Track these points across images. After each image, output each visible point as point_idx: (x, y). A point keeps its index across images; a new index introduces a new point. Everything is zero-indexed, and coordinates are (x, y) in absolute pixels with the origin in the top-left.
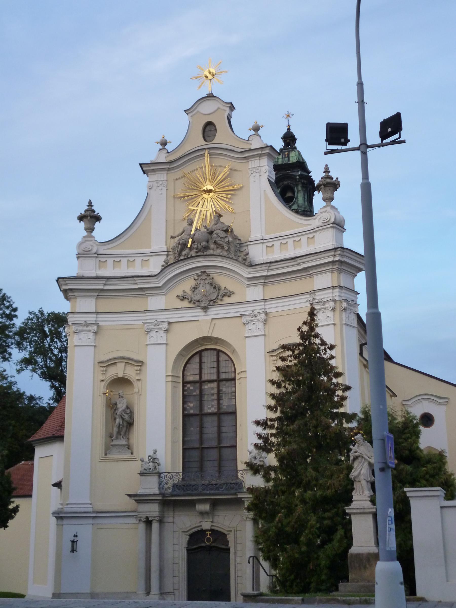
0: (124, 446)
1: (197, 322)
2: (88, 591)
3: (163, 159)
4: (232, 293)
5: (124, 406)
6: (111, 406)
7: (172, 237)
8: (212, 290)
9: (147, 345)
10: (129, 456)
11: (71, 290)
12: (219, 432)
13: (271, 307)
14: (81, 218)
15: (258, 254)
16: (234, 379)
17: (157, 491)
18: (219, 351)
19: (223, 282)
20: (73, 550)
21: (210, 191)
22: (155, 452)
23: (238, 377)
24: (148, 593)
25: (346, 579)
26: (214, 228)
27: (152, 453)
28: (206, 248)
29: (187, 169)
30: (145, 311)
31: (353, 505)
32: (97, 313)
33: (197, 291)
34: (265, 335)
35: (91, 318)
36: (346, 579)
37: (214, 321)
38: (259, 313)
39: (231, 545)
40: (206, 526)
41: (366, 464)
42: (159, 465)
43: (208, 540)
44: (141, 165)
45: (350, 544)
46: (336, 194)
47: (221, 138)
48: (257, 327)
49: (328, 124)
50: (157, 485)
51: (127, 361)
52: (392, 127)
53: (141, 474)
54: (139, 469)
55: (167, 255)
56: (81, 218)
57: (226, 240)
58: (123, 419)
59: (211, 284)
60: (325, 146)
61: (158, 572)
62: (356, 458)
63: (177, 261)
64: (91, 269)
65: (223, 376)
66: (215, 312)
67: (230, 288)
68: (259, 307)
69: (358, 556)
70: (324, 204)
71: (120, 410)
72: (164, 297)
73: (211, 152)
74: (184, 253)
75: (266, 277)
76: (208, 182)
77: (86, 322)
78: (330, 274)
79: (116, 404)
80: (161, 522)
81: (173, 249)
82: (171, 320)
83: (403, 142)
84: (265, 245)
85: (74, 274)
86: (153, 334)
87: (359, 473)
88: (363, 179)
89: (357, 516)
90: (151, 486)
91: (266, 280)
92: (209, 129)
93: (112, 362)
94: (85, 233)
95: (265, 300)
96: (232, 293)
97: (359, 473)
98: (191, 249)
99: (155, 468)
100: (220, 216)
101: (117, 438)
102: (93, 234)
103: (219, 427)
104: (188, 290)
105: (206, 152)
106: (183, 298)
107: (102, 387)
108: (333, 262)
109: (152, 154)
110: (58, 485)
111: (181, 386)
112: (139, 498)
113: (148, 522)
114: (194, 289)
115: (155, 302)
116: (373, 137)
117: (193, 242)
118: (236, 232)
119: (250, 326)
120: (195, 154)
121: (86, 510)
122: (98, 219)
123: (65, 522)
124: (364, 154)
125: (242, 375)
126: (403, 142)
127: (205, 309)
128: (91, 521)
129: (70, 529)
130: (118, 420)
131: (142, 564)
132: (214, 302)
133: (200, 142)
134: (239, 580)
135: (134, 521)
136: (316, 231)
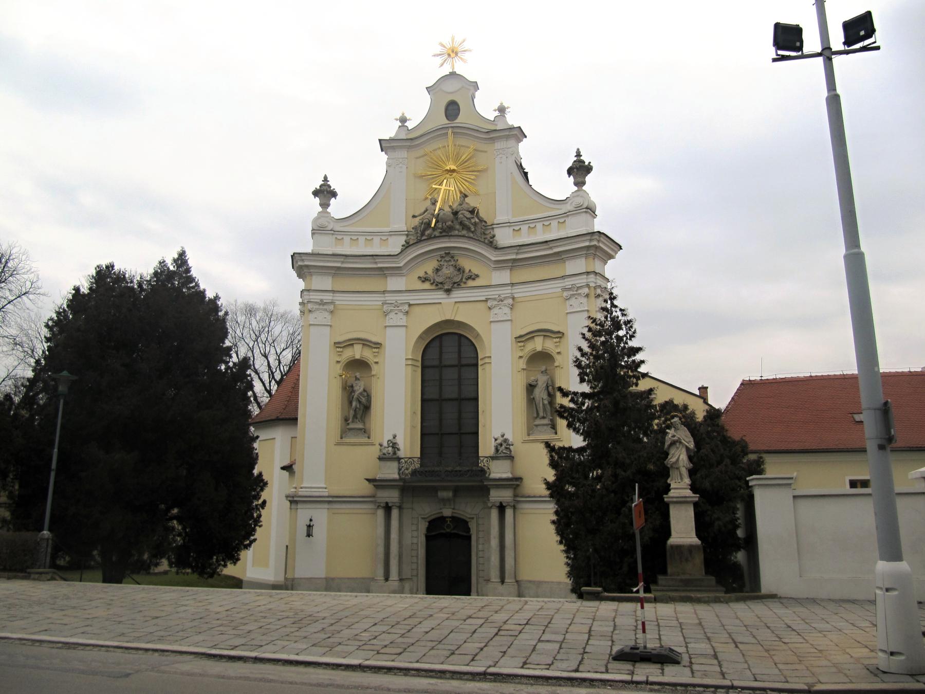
0: (360, 429)
1: (437, 306)
2: (323, 576)
3: (403, 136)
4: (477, 276)
5: (362, 389)
6: (348, 390)
7: (414, 216)
8: (456, 273)
9: (386, 327)
10: (366, 440)
11: (307, 266)
12: (460, 418)
13: (519, 292)
14: (316, 193)
15: (504, 237)
16: (476, 365)
17: (396, 476)
18: (460, 336)
19: (467, 264)
20: (309, 535)
21: (453, 171)
22: (395, 437)
23: (480, 363)
24: (387, 579)
25: (664, 572)
26: (459, 208)
27: (391, 438)
28: (451, 228)
29: (428, 148)
30: (384, 292)
31: (672, 493)
32: (333, 291)
33: (440, 273)
34: (331, 326)
35: (327, 297)
36: (664, 572)
37: (458, 305)
38: (506, 298)
39: (473, 532)
40: (447, 512)
41: (684, 450)
42: (399, 450)
43: (448, 526)
44: (380, 140)
45: (668, 534)
46: (588, 178)
47: (461, 119)
48: (503, 312)
49: (777, 26)
50: (396, 471)
51: (365, 343)
52: (860, 30)
53: (380, 459)
54: (378, 454)
55: (407, 235)
56: (316, 193)
57: (473, 221)
58: (360, 402)
59: (455, 266)
60: (772, 52)
61: (397, 558)
62: (673, 443)
63: (419, 241)
64: (328, 246)
65: (464, 362)
66: (458, 295)
67: (475, 271)
68: (507, 291)
69: (678, 548)
70: (576, 188)
71: (357, 393)
72: (404, 278)
73: (455, 130)
74: (427, 232)
75: (514, 260)
76: (451, 162)
77: (321, 300)
78: (583, 260)
79: (352, 386)
80: (400, 508)
81: (415, 228)
82: (411, 302)
83: (878, 48)
84: (512, 229)
85: (309, 250)
86: (392, 315)
87: (678, 460)
88: (829, 90)
89: (678, 506)
90: (391, 472)
91: (514, 264)
92: (452, 109)
93: (350, 343)
94: (320, 209)
95: (512, 284)
96: (477, 276)
97: (678, 460)
98: (434, 229)
99: (395, 453)
100: (466, 196)
101: (353, 422)
102: (329, 210)
103: (460, 412)
104: (430, 272)
105: (450, 131)
106: (424, 280)
107: (338, 369)
108: (588, 247)
109: (390, 131)
110: (288, 468)
111: (419, 370)
112: (377, 484)
113: (388, 509)
114: (437, 270)
115: (394, 283)
116: (837, 40)
117: (437, 222)
118: (482, 214)
119: (496, 311)
120: (438, 133)
121: (322, 494)
122: (334, 194)
123: (299, 506)
124: (828, 61)
125: (487, 360)
126: (878, 48)
127: (448, 291)
128: (326, 506)
129: (304, 514)
130: (354, 404)
131: (381, 550)
132: (457, 285)
133: (443, 121)
134: (481, 567)
135: (371, 506)
136: (568, 216)
